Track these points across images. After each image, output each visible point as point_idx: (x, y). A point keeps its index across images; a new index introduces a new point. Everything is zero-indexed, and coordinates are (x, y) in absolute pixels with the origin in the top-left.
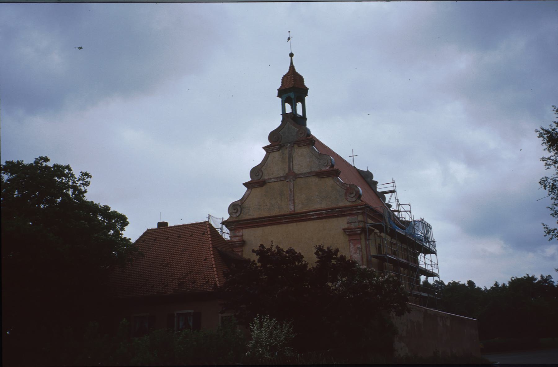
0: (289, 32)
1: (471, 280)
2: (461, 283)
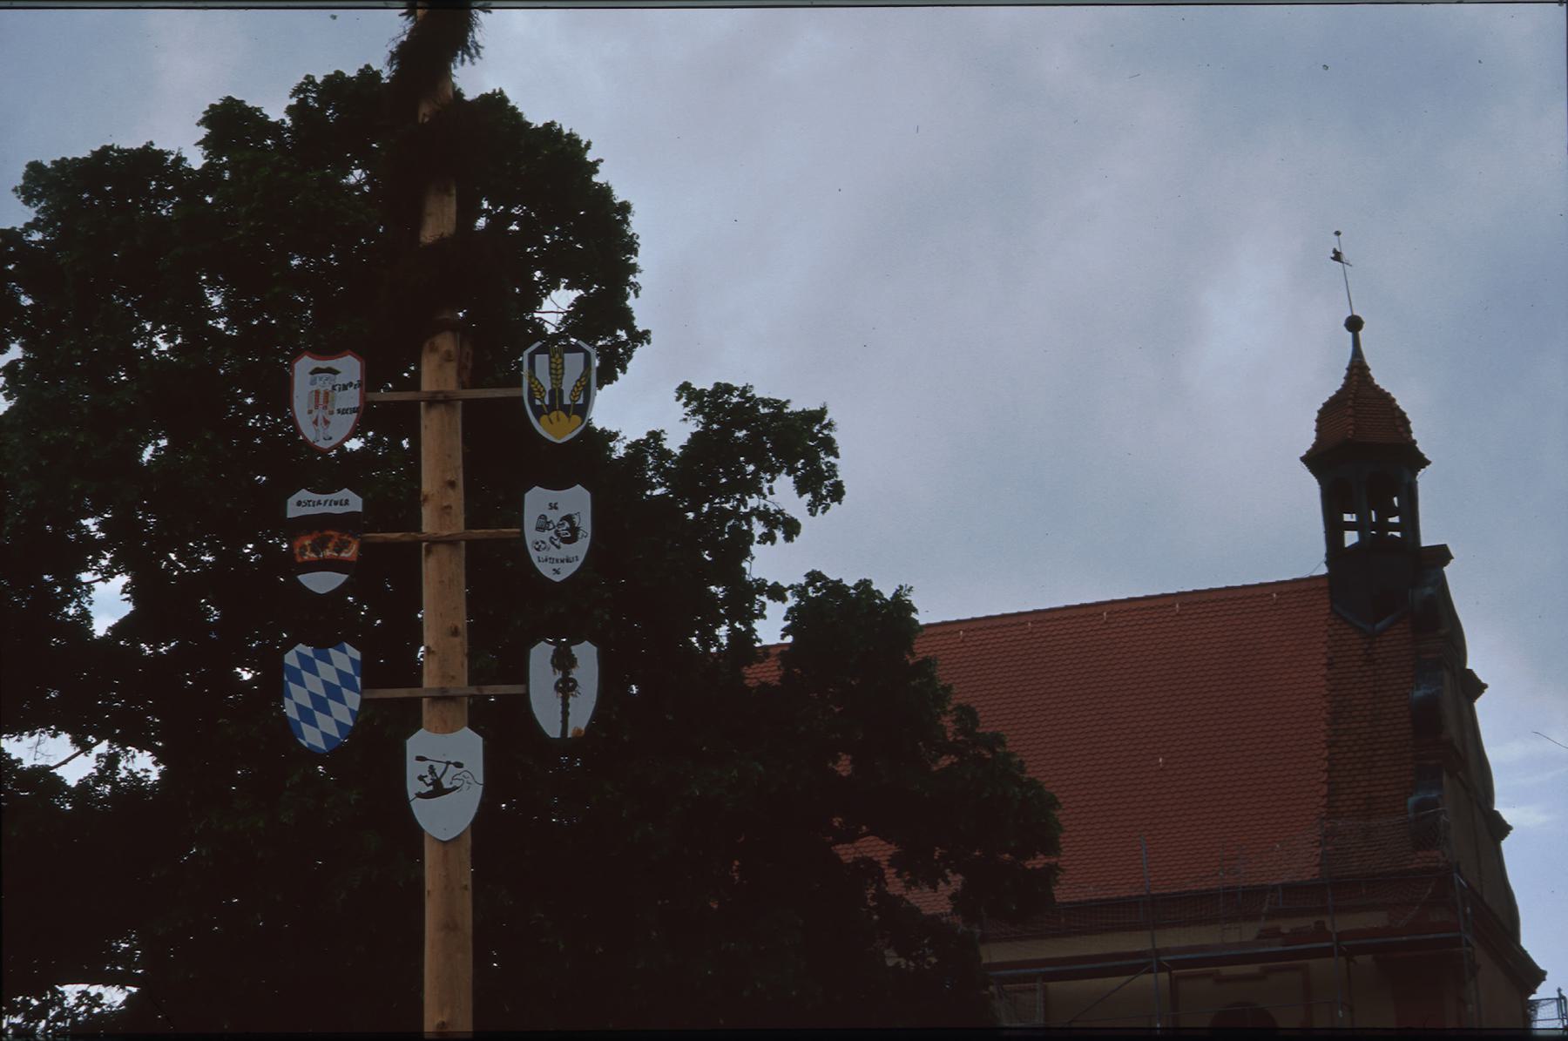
0: (1338, 233)
1: (1364, 325)
2: (636, 323)
